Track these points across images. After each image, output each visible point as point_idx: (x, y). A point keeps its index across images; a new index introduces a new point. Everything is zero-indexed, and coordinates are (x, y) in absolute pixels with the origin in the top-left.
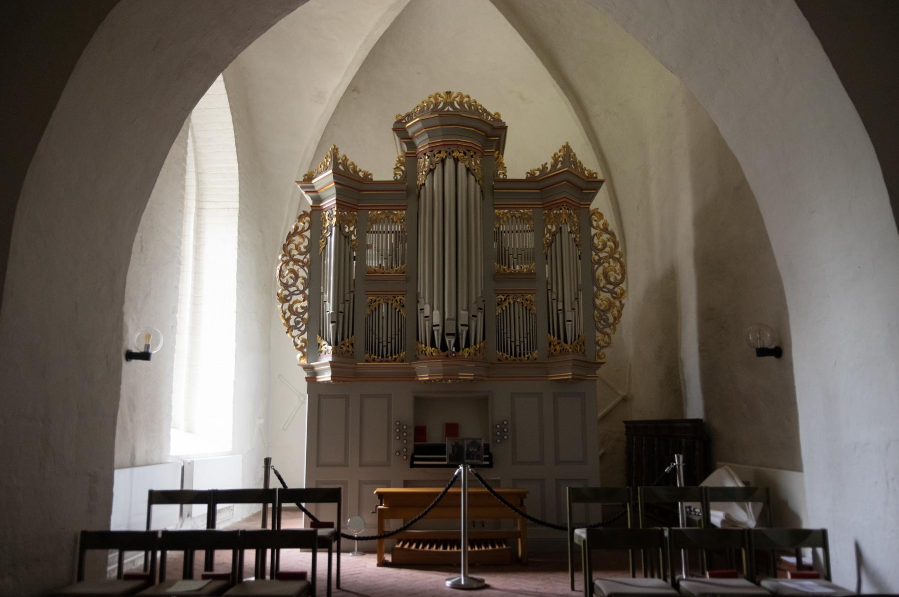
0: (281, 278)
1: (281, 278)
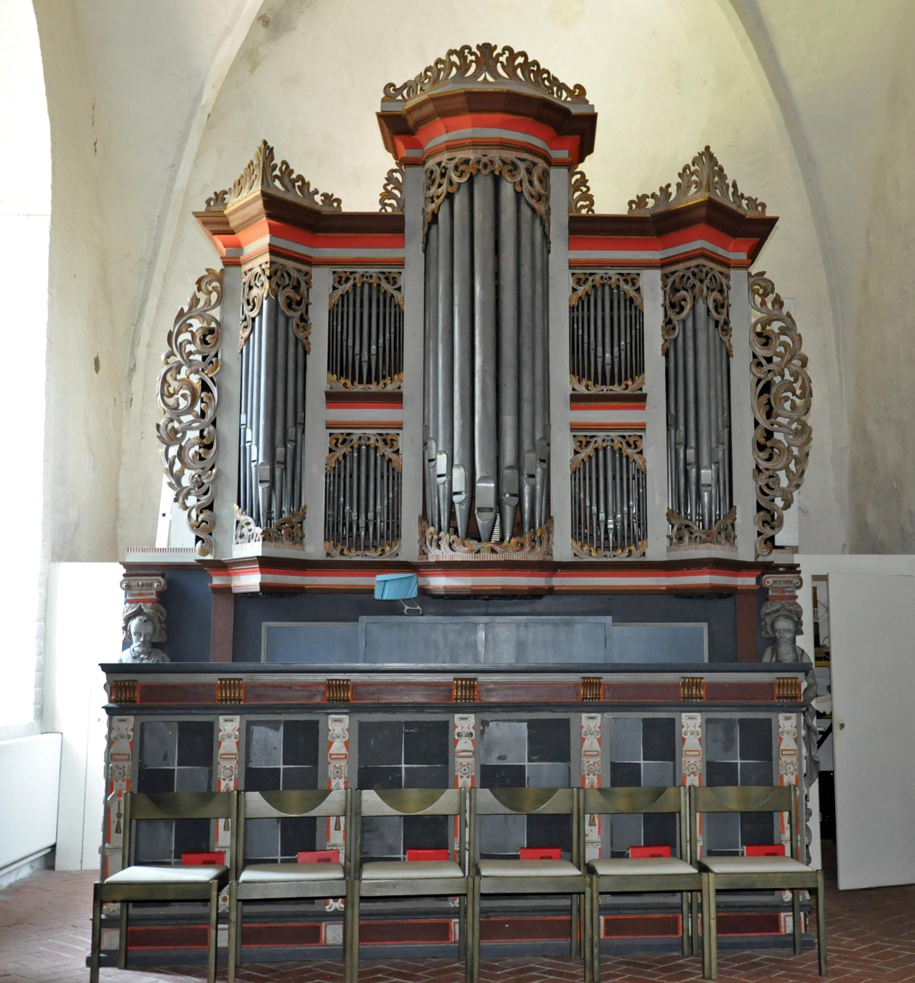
0: (165, 398)
1: (165, 398)
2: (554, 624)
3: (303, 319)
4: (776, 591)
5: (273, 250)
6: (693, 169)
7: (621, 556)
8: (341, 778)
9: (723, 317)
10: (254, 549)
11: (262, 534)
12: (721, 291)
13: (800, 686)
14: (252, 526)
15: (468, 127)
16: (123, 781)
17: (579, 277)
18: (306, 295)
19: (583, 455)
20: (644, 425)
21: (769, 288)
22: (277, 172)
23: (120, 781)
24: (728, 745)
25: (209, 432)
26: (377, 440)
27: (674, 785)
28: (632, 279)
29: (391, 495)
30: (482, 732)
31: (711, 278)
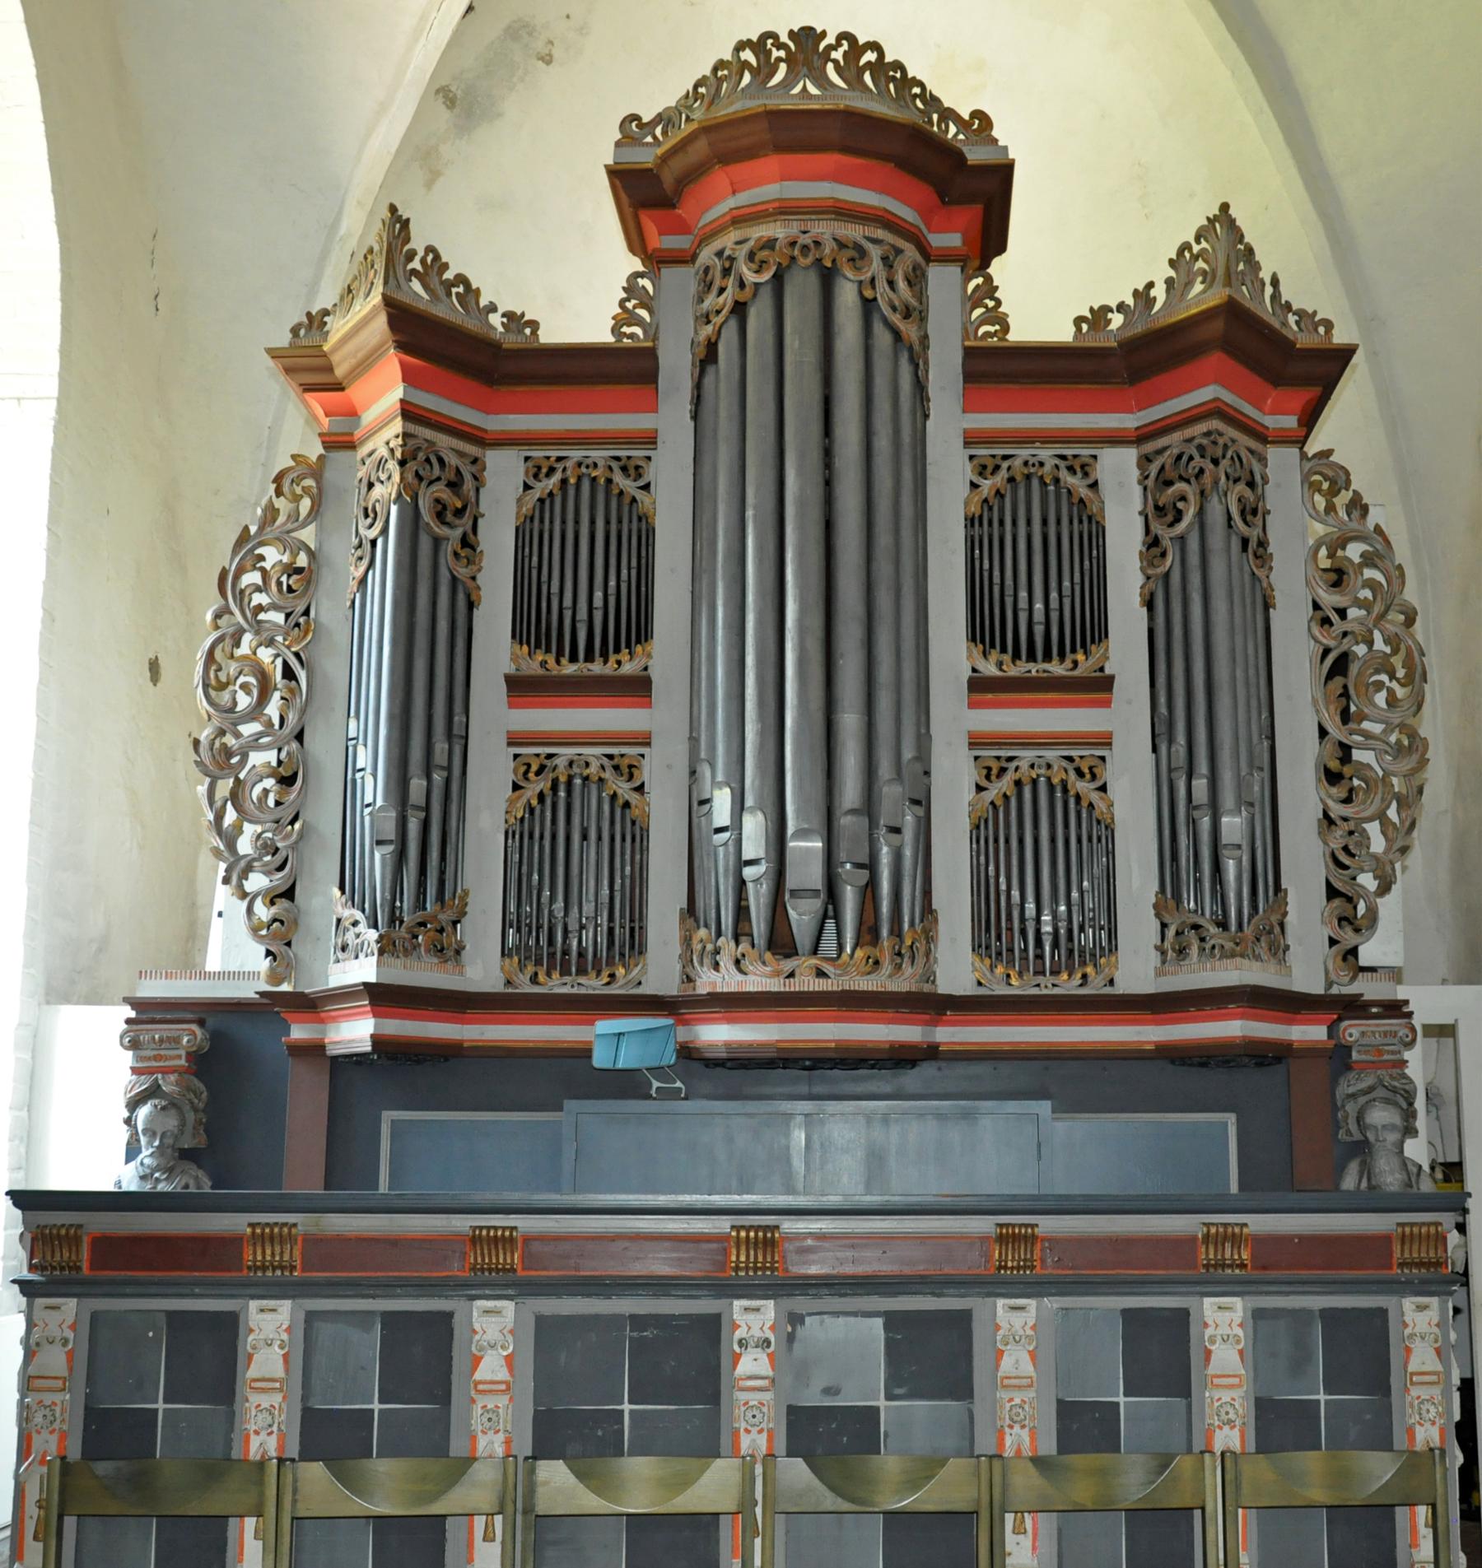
0: (213, 693)
1: (213, 693)
2: (940, 1117)
3: (468, 542)
4: (1366, 1052)
5: (409, 412)
6: (1196, 248)
7: (1068, 985)
8: (497, 1432)
9: (1255, 533)
10: (364, 970)
11: (378, 942)
12: (1251, 484)
13: (1445, 1239)
14: (362, 927)
15: (776, 182)
16: (52, 1432)
17: (983, 461)
18: (473, 500)
19: (994, 792)
20: (1109, 735)
21: (1339, 479)
22: (416, 264)
23: (45, 1434)
24: (1299, 1364)
25: (288, 753)
26: (603, 767)
27: (1189, 1451)
28: (1083, 467)
29: (628, 869)
30: (791, 1338)
31: (1232, 458)
